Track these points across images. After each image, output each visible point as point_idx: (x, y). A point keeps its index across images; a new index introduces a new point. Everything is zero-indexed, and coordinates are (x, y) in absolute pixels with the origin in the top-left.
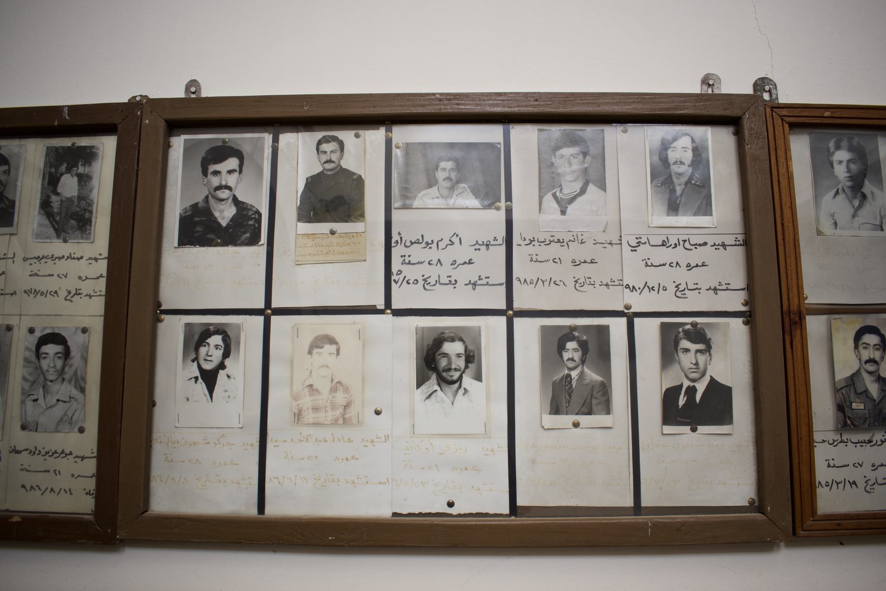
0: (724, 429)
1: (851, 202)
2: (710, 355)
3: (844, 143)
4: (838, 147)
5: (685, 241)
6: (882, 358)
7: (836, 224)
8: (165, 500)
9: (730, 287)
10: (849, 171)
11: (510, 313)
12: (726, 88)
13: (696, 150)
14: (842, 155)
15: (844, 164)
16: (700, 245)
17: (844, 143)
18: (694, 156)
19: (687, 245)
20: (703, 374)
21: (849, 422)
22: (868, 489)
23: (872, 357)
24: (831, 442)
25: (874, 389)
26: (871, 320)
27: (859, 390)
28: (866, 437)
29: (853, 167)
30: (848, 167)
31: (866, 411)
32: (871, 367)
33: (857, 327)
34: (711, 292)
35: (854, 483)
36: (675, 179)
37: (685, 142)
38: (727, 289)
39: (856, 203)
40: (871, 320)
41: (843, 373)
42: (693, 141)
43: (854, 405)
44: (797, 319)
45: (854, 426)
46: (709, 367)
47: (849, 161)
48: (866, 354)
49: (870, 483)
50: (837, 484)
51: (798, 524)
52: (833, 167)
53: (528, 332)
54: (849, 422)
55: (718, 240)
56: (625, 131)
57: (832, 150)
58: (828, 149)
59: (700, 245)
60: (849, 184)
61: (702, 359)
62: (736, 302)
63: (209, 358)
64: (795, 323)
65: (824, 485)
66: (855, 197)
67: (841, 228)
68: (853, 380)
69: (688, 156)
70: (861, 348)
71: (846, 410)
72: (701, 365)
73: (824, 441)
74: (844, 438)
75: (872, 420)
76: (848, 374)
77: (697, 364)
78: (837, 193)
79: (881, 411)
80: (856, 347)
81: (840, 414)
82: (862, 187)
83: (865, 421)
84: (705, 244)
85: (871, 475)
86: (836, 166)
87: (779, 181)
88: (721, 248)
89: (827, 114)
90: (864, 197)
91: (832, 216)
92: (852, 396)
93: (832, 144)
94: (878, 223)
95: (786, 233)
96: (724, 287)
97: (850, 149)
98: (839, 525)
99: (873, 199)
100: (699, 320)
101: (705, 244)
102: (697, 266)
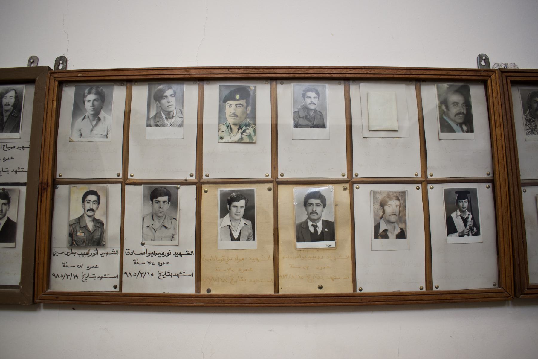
0: (12, 245)
1: (91, 122)
2: (9, 206)
3: (94, 91)
4: (89, 93)
5: (4, 146)
6: (97, 208)
7: (81, 135)
8: (59, 285)
9: (23, 170)
10: (93, 105)
11: (424, 182)
12: (42, 64)
13: (16, 97)
14: (91, 97)
15: (91, 102)
16: (12, 148)
17: (94, 91)
18: (15, 101)
19: (5, 148)
20: (4, 216)
21: (74, 243)
22: (83, 279)
23: (91, 207)
24: (66, 253)
25: (90, 225)
26: (93, 187)
27: (82, 226)
28: (85, 251)
29: (96, 103)
30: (93, 104)
31: (85, 237)
32: (90, 213)
33: (85, 191)
34: (14, 173)
35: (77, 276)
36: (4, 113)
37: (12, 93)
38: (22, 171)
39: (94, 123)
40: (93, 187)
41: (74, 216)
42: (16, 93)
43: (79, 234)
44: (46, 187)
45: (77, 245)
46: (8, 212)
47: (94, 100)
48: (88, 206)
49: (85, 276)
50: (67, 276)
51: (35, 296)
52: (84, 104)
53: (437, 195)
54: (74, 243)
55: (21, 145)
56: (506, 64)
57: (86, 94)
58: (84, 94)
59: (12, 148)
60: (92, 113)
61: (4, 207)
62: (23, 178)
63: (161, 210)
64: (44, 189)
65: (60, 276)
66: (94, 120)
67: (83, 137)
68: (79, 220)
69: (13, 101)
70: (86, 203)
71: (74, 236)
72: (4, 211)
73: (62, 253)
74: (73, 251)
75: (87, 242)
76: (77, 217)
77: (2, 210)
78: (85, 118)
79: (93, 237)
80: (83, 202)
81: (70, 238)
82: (99, 115)
83: (84, 242)
84: (14, 147)
85: (86, 272)
86: (86, 103)
87: (47, 113)
88: (22, 149)
89: (80, 75)
90: (99, 119)
91: (80, 130)
92: (78, 228)
93: (86, 91)
94: (105, 134)
95: (46, 141)
96: (21, 170)
97: (97, 93)
98: (57, 297)
99: (104, 120)
100: (6, 187)
101: (14, 147)
102: (8, 159)
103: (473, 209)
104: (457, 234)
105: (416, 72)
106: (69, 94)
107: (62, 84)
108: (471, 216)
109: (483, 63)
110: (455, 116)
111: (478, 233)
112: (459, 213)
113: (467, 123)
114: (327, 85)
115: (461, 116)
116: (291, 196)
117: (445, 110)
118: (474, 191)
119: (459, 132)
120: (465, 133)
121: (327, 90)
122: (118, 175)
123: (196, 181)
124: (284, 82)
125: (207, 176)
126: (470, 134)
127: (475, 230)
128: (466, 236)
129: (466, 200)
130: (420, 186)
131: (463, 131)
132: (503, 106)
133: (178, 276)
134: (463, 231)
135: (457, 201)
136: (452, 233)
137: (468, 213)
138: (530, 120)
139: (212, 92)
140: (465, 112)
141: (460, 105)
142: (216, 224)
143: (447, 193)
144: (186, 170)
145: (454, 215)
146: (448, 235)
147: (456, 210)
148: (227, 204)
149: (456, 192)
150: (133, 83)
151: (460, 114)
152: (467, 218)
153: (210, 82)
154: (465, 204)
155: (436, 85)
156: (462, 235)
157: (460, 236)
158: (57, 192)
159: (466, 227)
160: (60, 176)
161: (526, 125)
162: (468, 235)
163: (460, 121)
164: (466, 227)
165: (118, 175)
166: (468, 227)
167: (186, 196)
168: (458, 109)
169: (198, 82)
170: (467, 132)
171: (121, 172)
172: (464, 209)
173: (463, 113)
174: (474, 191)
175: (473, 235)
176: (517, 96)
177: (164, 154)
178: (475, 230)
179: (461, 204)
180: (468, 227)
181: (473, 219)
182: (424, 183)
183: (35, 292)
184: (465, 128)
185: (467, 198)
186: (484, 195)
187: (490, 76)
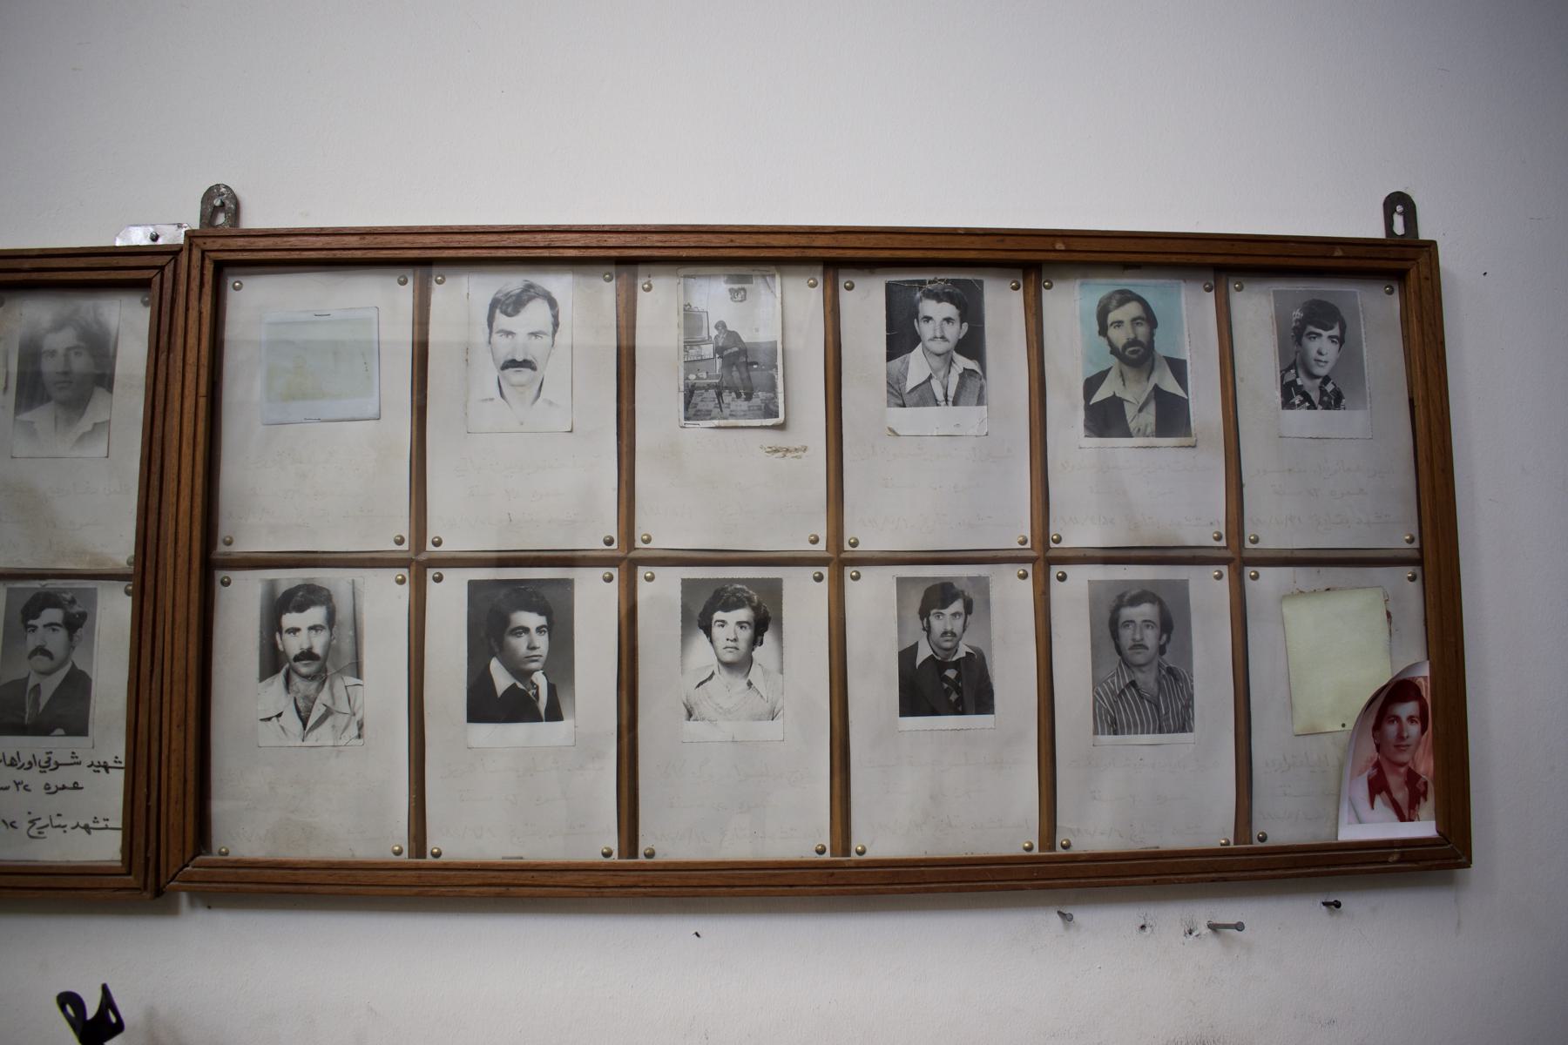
11: (419, 564)
89: (1338, 253)
114: (1183, 284)
121: (1183, 299)
125: (1219, 538)
130: (825, 571)
133: (87, 828)
142: (679, 665)
144: (803, 530)
148: (700, 614)
158: (223, 596)
160: (1219, 538)
165: (815, 541)
167: (805, 598)
176: (866, 302)
177: (523, 476)
182: (624, 564)
183: (171, 856)
186: (114, 612)
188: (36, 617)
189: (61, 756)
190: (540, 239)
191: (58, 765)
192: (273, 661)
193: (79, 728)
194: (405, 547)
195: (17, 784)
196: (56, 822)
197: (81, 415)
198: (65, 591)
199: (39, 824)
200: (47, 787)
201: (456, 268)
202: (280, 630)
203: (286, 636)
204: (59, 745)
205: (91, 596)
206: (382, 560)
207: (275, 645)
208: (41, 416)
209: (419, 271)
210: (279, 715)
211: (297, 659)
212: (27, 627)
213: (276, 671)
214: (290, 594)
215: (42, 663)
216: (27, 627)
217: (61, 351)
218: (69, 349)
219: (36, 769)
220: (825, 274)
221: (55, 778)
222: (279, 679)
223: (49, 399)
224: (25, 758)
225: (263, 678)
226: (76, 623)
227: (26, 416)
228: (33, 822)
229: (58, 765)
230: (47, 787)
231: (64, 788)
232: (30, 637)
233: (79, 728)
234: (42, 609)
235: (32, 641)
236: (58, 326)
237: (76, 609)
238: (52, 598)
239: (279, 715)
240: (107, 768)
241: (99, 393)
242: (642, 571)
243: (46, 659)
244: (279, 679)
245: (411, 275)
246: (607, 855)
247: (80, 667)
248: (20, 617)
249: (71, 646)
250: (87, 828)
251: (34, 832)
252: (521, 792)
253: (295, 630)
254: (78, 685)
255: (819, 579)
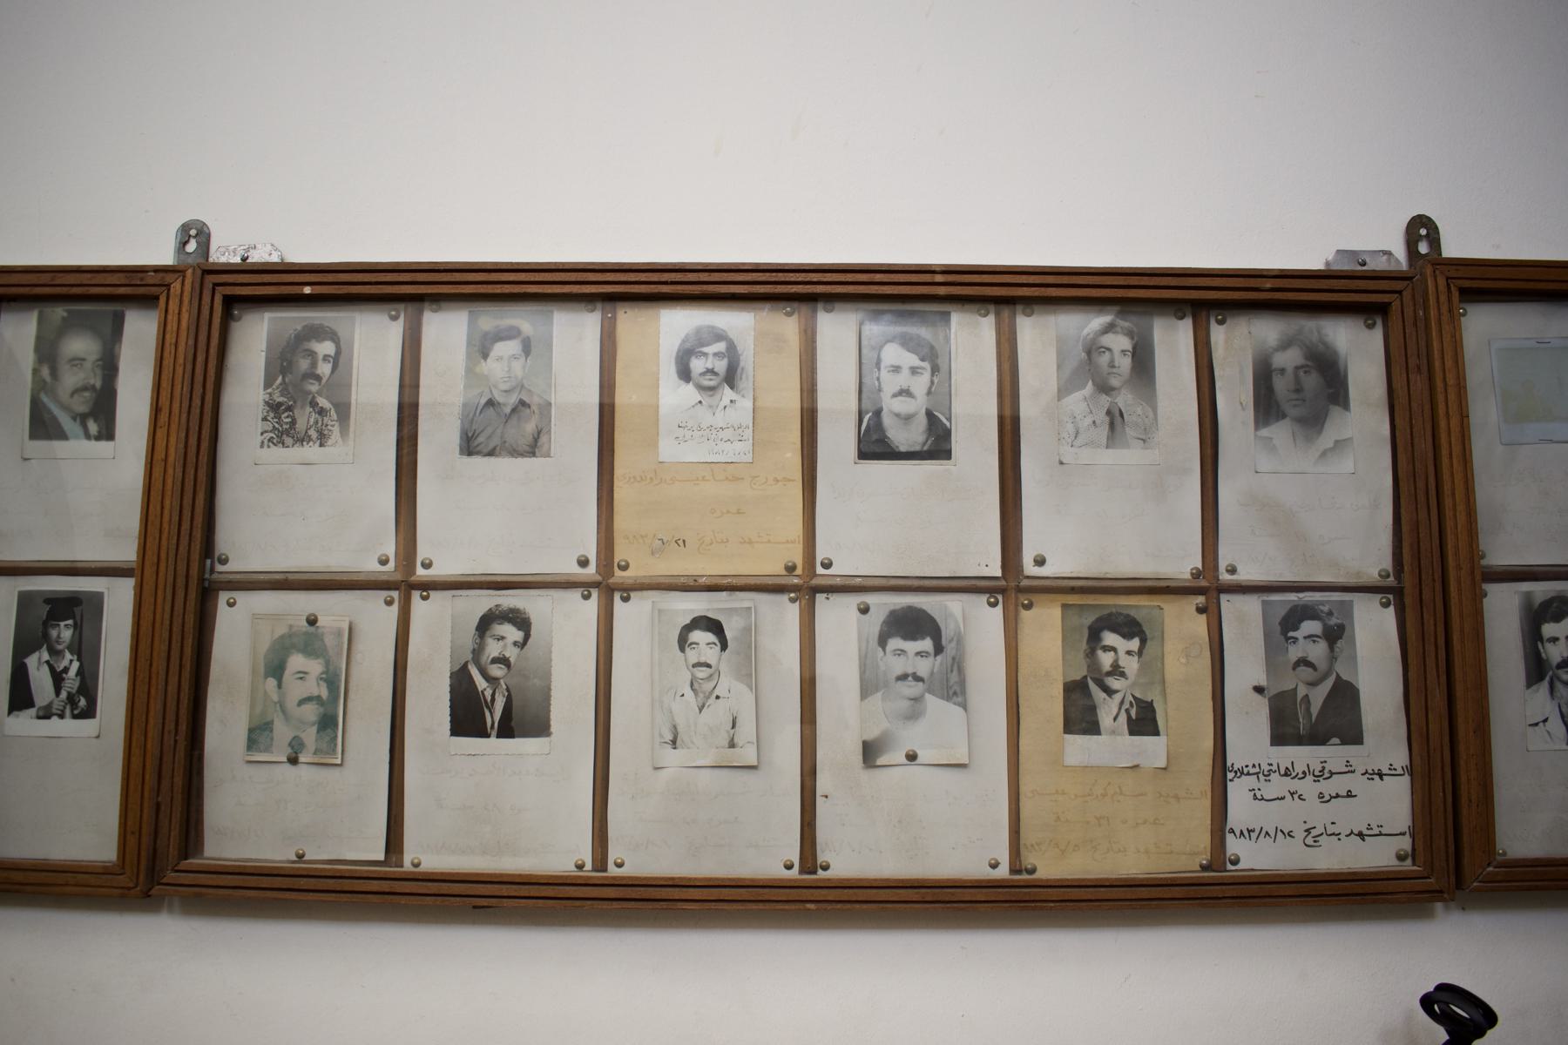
26: (509, 600)
40: (509, 600)
103: (86, 649)
104: (32, 711)
105: (71, 279)
106: (255, 338)
107: (235, 304)
108: (76, 665)
109: (1423, 248)
110: (72, 395)
111: (89, 713)
112: (46, 656)
113: (101, 413)
115: (87, 394)
116: (439, 627)
117: (48, 379)
118: (96, 600)
119: (77, 437)
120: (93, 442)
122: (384, 562)
123: (398, 577)
124: (837, 305)
126: (103, 444)
127: (83, 702)
128: (55, 718)
129: (70, 622)
130: (395, 594)
131: (88, 436)
132: (189, 367)
133: (1361, 835)
134: (50, 706)
135: (45, 624)
136: (20, 709)
137: (68, 656)
138: (280, 404)
139: (1042, 338)
140: (98, 385)
141: (88, 365)
143: (25, 600)
145: (32, 661)
146: (10, 712)
147: (37, 648)
149: (47, 601)
150: (426, 304)
151: (85, 389)
152: (66, 670)
153: (443, 304)
154: (64, 632)
155: (795, 317)
156: (46, 714)
157: (39, 717)
159: (58, 693)
161: (265, 419)
162: (62, 716)
163: (82, 409)
164: (58, 693)
166: (64, 695)
168: (82, 375)
169: (599, 305)
170: (98, 438)
171: (390, 550)
172: (60, 647)
173: (93, 387)
174: (96, 600)
175: (75, 717)
178: (83, 702)
179: (54, 633)
180: (64, 695)
181: (80, 672)
184: (93, 427)
185: (74, 618)
187: (168, 286)
188: (1296, 628)
189: (1335, 765)
190: (71, 279)
191: (1332, 774)
192: (1537, 669)
193: (1353, 735)
194: (391, 566)
195: (1292, 794)
196: (1331, 829)
197: (1320, 431)
198: (1322, 603)
199: (1314, 833)
200: (1321, 796)
201: (654, 304)
202: (1541, 639)
203: (1549, 646)
204: (1333, 754)
205: (1347, 609)
206: (293, 582)
207: (1538, 654)
208: (1280, 432)
209: (411, 307)
210: (1545, 721)
211: (1559, 666)
212: (1287, 639)
213: (1541, 678)
214: (1547, 604)
215: (1305, 672)
216: (1287, 639)
217: (1290, 370)
218: (1297, 368)
219: (1310, 778)
220: (997, 314)
221: (1329, 787)
222: (1546, 683)
223: (1284, 416)
224: (1299, 768)
225: (1529, 685)
226: (1335, 635)
227: (1264, 432)
228: (1308, 831)
229: (1332, 774)
230: (1321, 796)
231: (1337, 796)
232: (1292, 649)
233: (1353, 735)
234: (1301, 621)
235: (1295, 653)
236: (1285, 345)
237: (1333, 621)
238: (56, 616)
239: (1545, 721)
240: (1381, 776)
241: (1335, 411)
242: (416, 595)
243: (1310, 670)
244: (1544, 686)
245: (403, 310)
246: (580, 867)
247: (1345, 677)
248: (1278, 628)
249: (1333, 658)
250: (1361, 835)
251: (1310, 841)
252: (518, 803)
253: (1554, 640)
254: (1345, 695)
255: (389, 603)
